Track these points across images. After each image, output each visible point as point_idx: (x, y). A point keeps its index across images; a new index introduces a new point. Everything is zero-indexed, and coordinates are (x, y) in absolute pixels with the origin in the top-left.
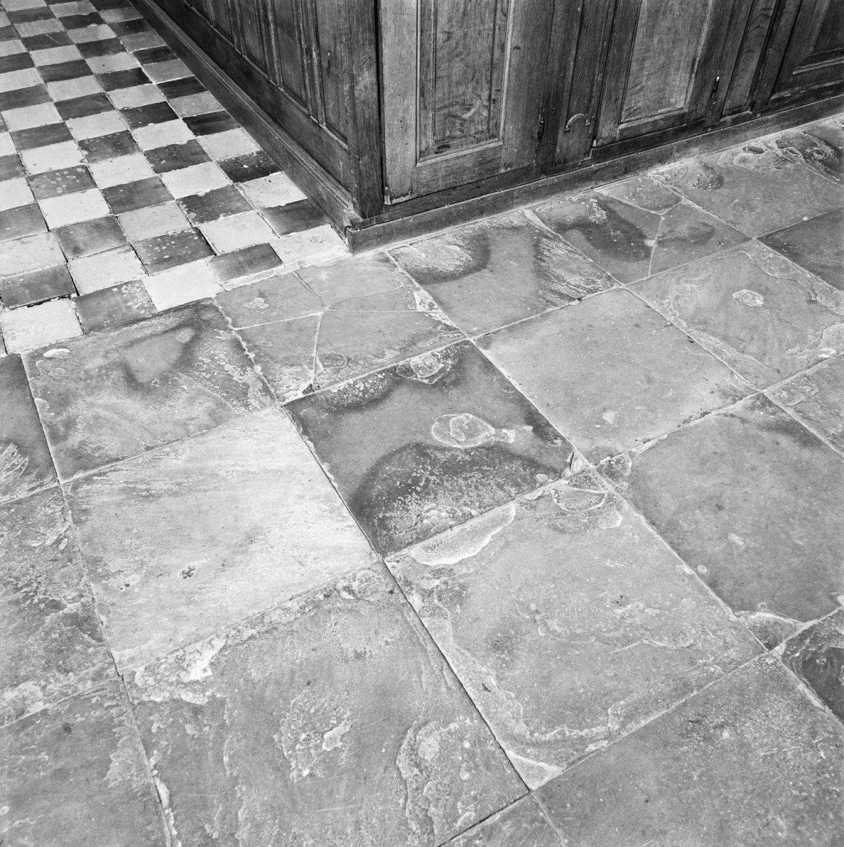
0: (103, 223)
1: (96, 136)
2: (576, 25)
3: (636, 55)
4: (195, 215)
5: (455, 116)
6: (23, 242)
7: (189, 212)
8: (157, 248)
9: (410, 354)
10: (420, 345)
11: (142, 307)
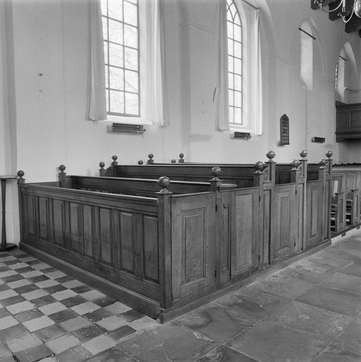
0: (54, 327)
1: (36, 298)
2: (222, 240)
3: (237, 249)
4: (92, 319)
5: (191, 270)
6: (21, 338)
7: (89, 319)
8: (82, 333)
9: (205, 353)
10: (206, 349)
11: (86, 355)
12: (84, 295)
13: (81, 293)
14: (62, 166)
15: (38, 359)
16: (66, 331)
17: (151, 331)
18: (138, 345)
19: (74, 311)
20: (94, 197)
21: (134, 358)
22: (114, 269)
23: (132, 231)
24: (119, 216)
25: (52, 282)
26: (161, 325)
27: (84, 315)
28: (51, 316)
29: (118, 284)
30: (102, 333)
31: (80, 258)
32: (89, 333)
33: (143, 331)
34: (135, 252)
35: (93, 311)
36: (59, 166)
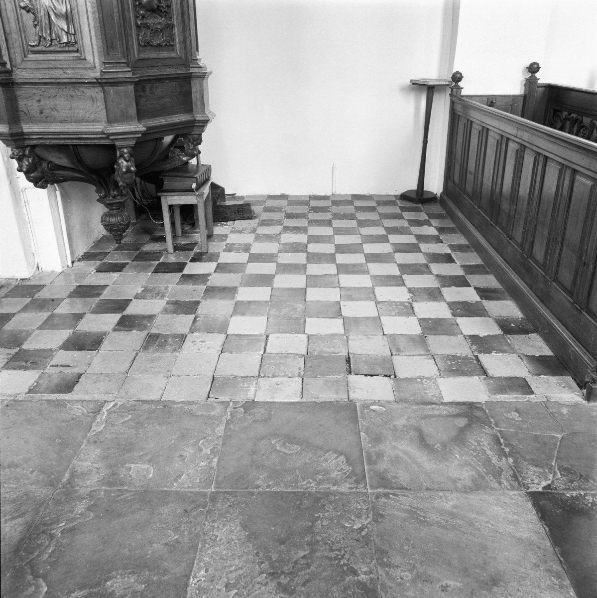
7: (472, 344)
8: (449, 362)
11: (434, 396)
12: (489, 305)
13: (486, 299)
14: (535, 63)
15: (372, 373)
16: (428, 350)
17: (560, 405)
18: (519, 417)
19: (457, 325)
20: (540, 134)
21: (498, 434)
22: (544, 277)
23: (587, 213)
24: (572, 181)
25: (454, 270)
26: (585, 402)
27: (468, 336)
28: (422, 321)
29: (545, 305)
30: (476, 375)
31: (505, 241)
32: (458, 367)
33: (545, 399)
34: (581, 257)
35: (486, 334)
36: (528, 65)
